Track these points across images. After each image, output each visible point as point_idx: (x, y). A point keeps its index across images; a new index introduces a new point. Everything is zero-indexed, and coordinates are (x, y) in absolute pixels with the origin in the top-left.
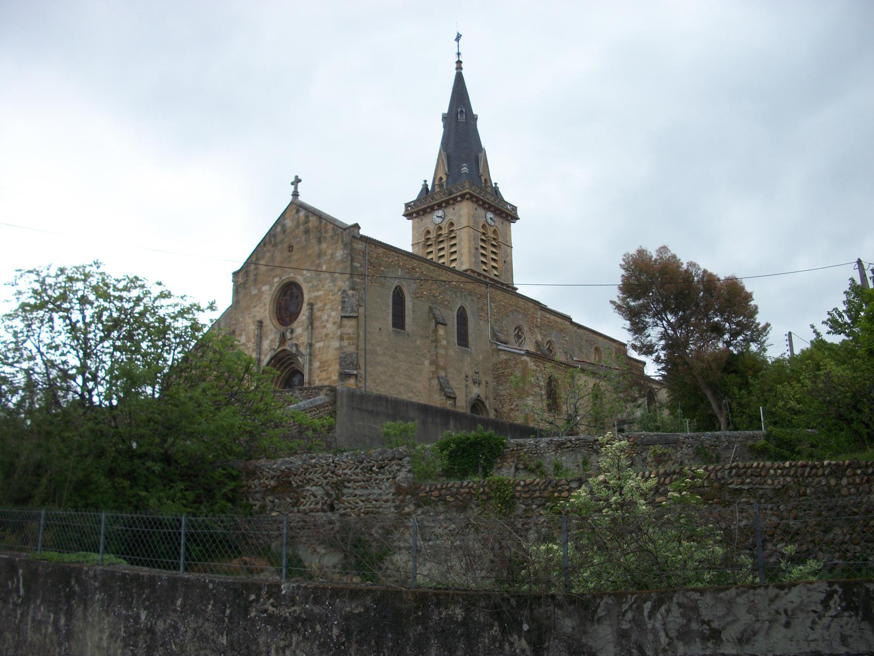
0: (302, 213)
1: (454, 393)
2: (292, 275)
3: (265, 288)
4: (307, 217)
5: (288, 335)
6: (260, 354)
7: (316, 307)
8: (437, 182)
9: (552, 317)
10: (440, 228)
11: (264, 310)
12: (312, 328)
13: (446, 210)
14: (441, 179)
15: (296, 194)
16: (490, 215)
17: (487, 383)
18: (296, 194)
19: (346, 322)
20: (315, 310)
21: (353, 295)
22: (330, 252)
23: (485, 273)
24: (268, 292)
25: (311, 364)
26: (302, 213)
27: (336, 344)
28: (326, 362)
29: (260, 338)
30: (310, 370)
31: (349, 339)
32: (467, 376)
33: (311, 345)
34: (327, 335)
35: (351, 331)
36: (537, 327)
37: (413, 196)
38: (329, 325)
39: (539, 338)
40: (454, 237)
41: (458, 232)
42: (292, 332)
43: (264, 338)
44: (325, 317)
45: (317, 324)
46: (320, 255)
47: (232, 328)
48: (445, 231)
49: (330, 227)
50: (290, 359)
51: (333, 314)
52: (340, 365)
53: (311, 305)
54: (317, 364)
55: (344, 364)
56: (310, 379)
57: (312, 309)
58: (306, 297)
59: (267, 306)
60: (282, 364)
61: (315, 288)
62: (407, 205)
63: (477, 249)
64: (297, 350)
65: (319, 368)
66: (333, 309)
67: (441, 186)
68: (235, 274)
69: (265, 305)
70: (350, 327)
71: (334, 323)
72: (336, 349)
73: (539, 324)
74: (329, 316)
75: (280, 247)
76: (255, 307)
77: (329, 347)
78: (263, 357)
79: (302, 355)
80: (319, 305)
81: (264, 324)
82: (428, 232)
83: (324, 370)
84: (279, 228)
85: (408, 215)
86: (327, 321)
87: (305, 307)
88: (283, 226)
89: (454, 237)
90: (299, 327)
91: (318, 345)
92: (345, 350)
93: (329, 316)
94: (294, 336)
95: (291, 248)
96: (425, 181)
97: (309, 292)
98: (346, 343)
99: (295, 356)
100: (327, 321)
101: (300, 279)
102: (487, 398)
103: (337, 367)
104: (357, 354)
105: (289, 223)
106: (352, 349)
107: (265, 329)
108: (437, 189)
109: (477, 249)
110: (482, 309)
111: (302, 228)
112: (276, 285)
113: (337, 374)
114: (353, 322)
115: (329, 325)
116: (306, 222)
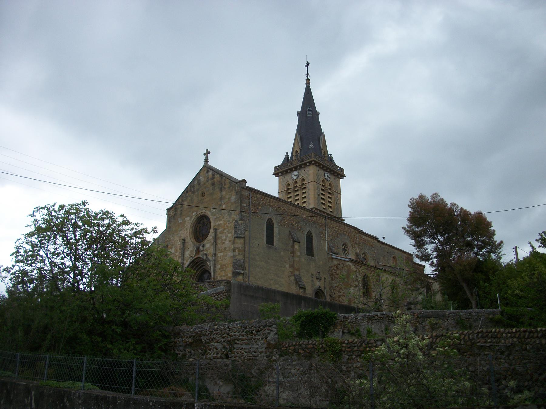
0: (210, 173)
1: (304, 285)
2: (204, 211)
3: (187, 219)
4: (213, 175)
5: (201, 248)
6: (183, 260)
7: (218, 231)
8: (294, 154)
9: (366, 238)
10: (296, 182)
11: (186, 232)
12: (216, 244)
13: (300, 171)
14: (297, 151)
15: (206, 161)
16: (327, 174)
17: (325, 279)
18: (206, 161)
19: (237, 240)
20: (218, 233)
21: (242, 224)
22: (227, 197)
23: (324, 210)
24: (189, 221)
25: (215, 266)
26: (210, 173)
27: (231, 254)
28: (224, 265)
29: (183, 250)
30: (214, 270)
31: (239, 251)
32: (312, 275)
33: (215, 255)
34: (225, 249)
35: (240, 246)
36: (356, 244)
37: (279, 162)
38: (227, 242)
39: (358, 251)
40: (305, 188)
41: (307, 185)
42: (203, 246)
43: (186, 250)
44: (224, 237)
45: (219, 241)
46: (221, 199)
47: (166, 243)
48: (299, 184)
49: (228, 181)
50: (203, 265)
51: (229, 235)
52: (233, 267)
53: (216, 230)
54: (219, 266)
55: (236, 266)
56: (214, 276)
57: (216, 232)
58: (212, 225)
59: (188, 230)
60: (197, 266)
61: (218, 219)
62: (276, 168)
63: (319, 195)
64: (207, 258)
65: (220, 269)
66: (229, 233)
67: (297, 156)
68: (168, 210)
69: (187, 229)
70: (239, 243)
71: (230, 241)
72: (231, 257)
73: (358, 242)
74: (227, 236)
75: (196, 193)
76: (181, 230)
77: (226, 256)
78: (185, 262)
79: (210, 261)
80: (220, 230)
81: (186, 241)
82: (289, 185)
83: (223, 270)
84: (196, 182)
85: (276, 174)
86: (225, 240)
87: (212, 231)
88: (199, 181)
89: (305, 188)
90: (208, 244)
91: (220, 255)
92: (237, 258)
93: (227, 236)
94: (205, 248)
95: (203, 194)
96: (287, 153)
97: (214, 221)
98: (237, 253)
99: (205, 261)
100: (225, 240)
101: (208, 214)
102: (325, 288)
103: (231, 268)
104: (244, 260)
105: (202, 179)
106: (241, 257)
107: (186, 244)
108: (294, 158)
109: (319, 195)
110: (322, 233)
111: (210, 182)
112: (194, 217)
113: (231, 273)
114: (242, 240)
115: (227, 242)
116: (213, 178)
